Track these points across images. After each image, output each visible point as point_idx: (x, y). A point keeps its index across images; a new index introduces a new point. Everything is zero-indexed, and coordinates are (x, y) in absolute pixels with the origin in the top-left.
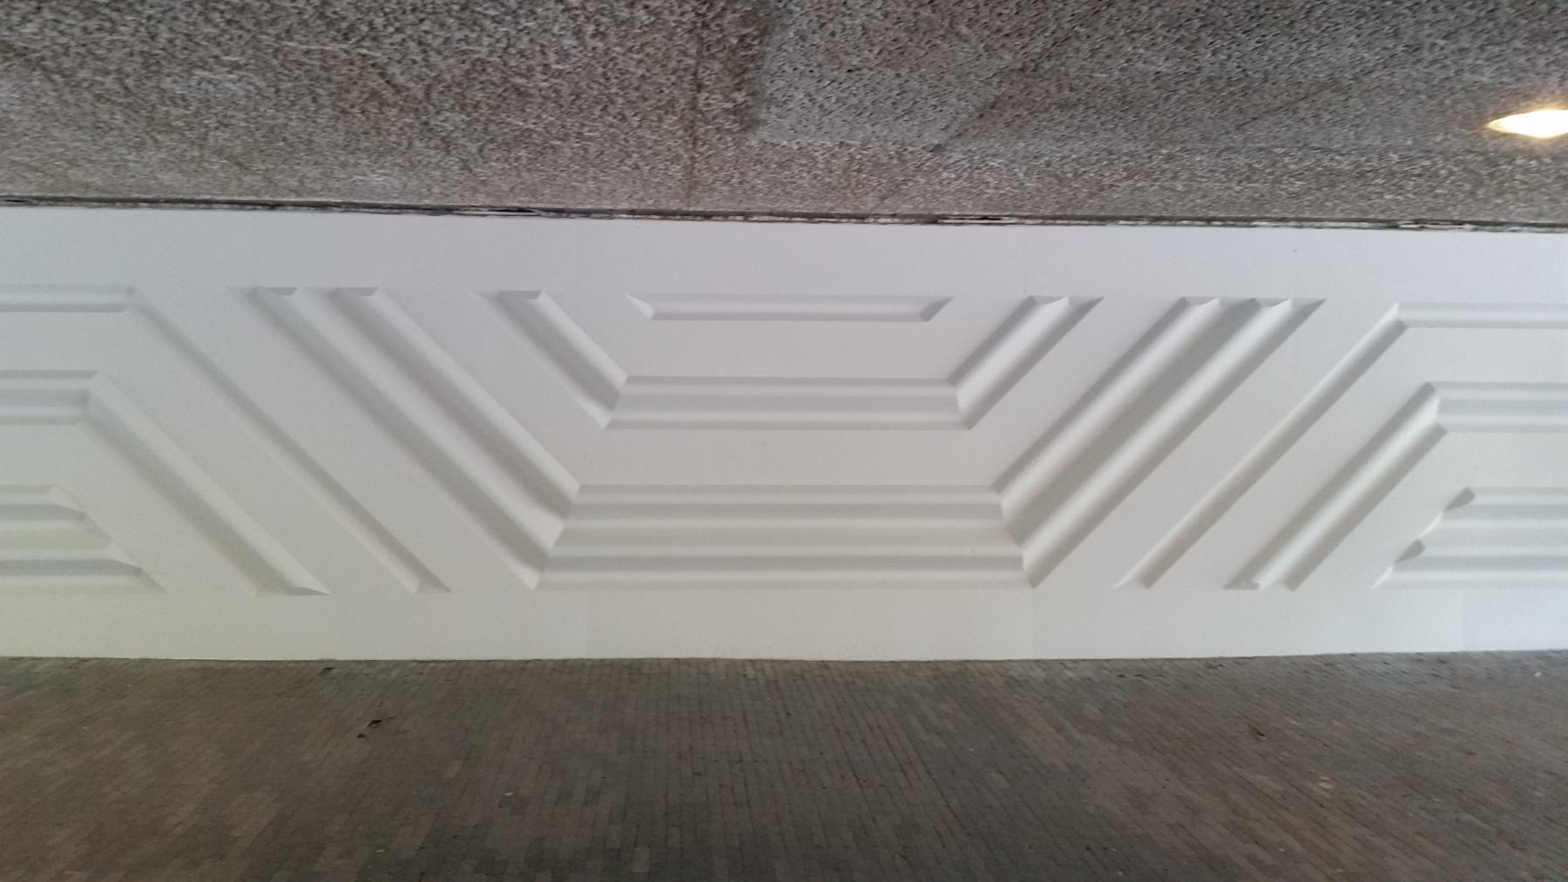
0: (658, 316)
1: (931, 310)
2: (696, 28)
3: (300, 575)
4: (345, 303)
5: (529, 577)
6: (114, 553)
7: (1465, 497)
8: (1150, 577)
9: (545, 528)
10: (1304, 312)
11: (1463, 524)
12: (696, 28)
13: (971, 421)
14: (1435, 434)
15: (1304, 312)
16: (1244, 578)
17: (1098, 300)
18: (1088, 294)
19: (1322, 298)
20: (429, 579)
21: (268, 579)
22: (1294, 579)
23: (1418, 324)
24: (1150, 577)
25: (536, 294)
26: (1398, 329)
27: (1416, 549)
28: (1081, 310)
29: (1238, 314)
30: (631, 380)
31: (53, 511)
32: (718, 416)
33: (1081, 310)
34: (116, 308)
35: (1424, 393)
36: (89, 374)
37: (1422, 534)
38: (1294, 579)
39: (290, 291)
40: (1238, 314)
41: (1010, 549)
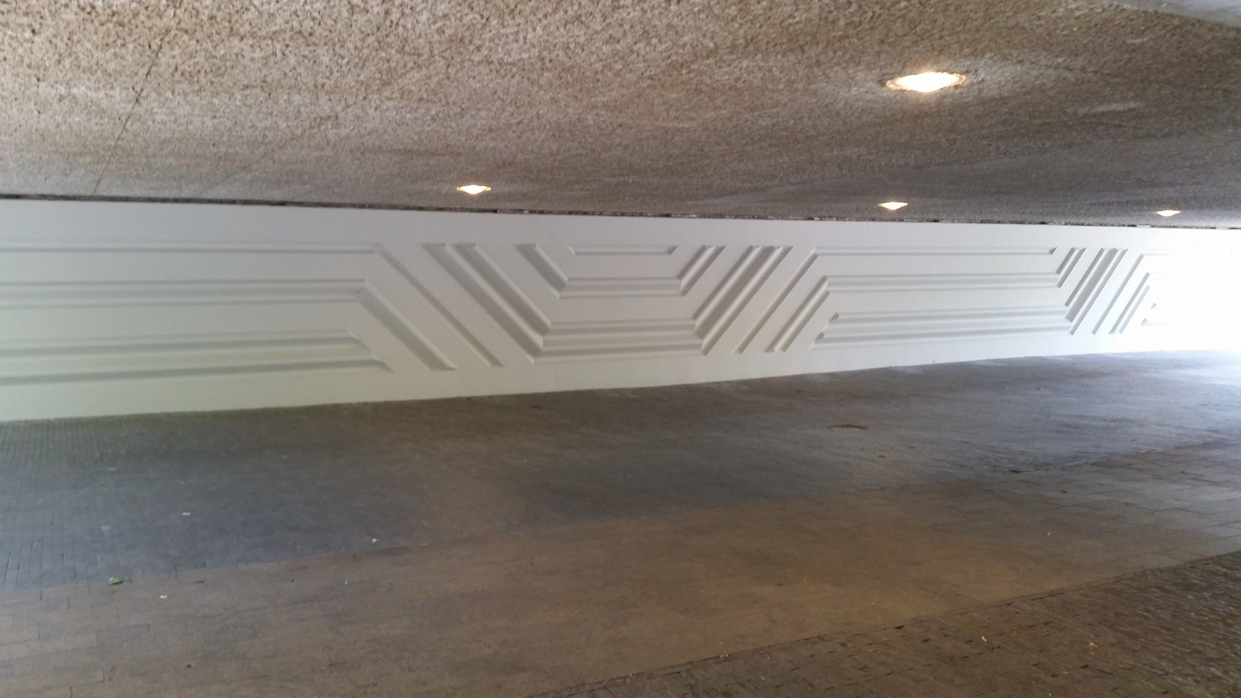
0: (577, 253)
1: (671, 251)
2: (1034, 133)
3: (452, 365)
4: (465, 251)
5: (532, 360)
6: (374, 356)
7: (836, 316)
8: (741, 350)
9: (538, 339)
10: (787, 251)
11: (837, 326)
12: (1034, 133)
13: (684, 293)
14: (826, 294)
15: (787, 251)
16: (770, 348)
17: (791, 248)
18: (721, 245)
19: (1055, 247)
20: (495, 362)
21: (436, 364)
22: (785, 348)
23: (821, 254)
24: (741, 350)
25: (474, 245)
26: (815, 257)
27: (821, 336)
28: (719, 251)
29: (768, 251)
30: (570, 279)
31: (349, 340)
32: (582, 293)
33: (719, 251)
34: (372, 252)
35: (824, 279)
36: (363, 281)
37: (823, 330)
38: (785, 348)
39: (474, 245)
40: (768, 251)
41: (697, 341)
